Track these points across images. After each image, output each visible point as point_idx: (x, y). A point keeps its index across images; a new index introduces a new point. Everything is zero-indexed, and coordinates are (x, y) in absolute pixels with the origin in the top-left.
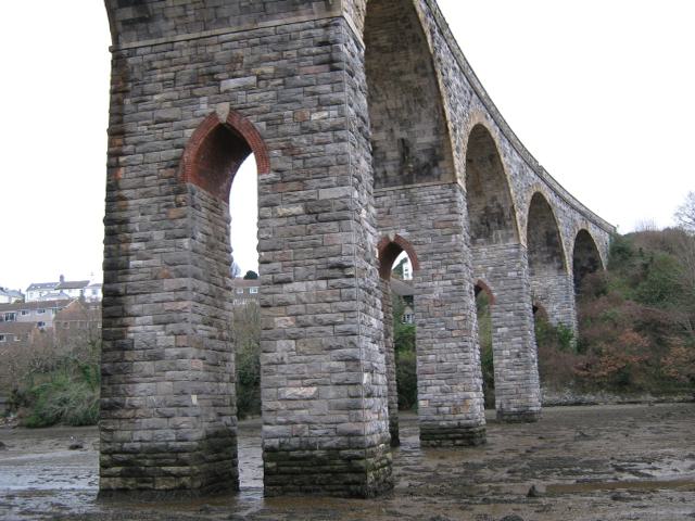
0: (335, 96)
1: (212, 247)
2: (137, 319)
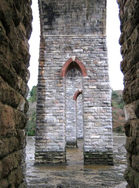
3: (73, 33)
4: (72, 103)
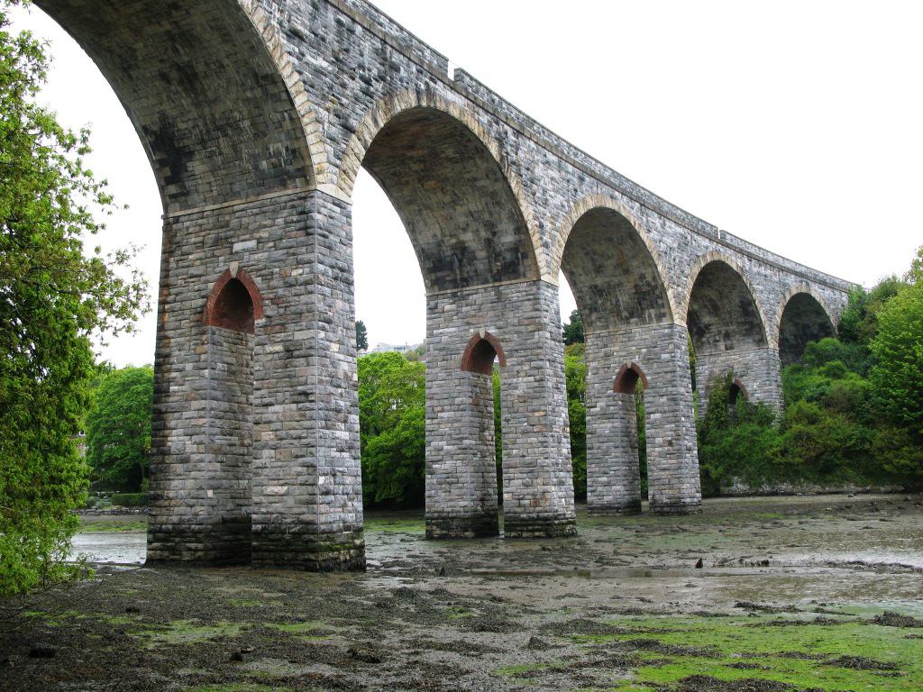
0: (306, 257)
1: (233, 373)
2: (174, 431)
3: (236, 195)
4: (457, 381)
